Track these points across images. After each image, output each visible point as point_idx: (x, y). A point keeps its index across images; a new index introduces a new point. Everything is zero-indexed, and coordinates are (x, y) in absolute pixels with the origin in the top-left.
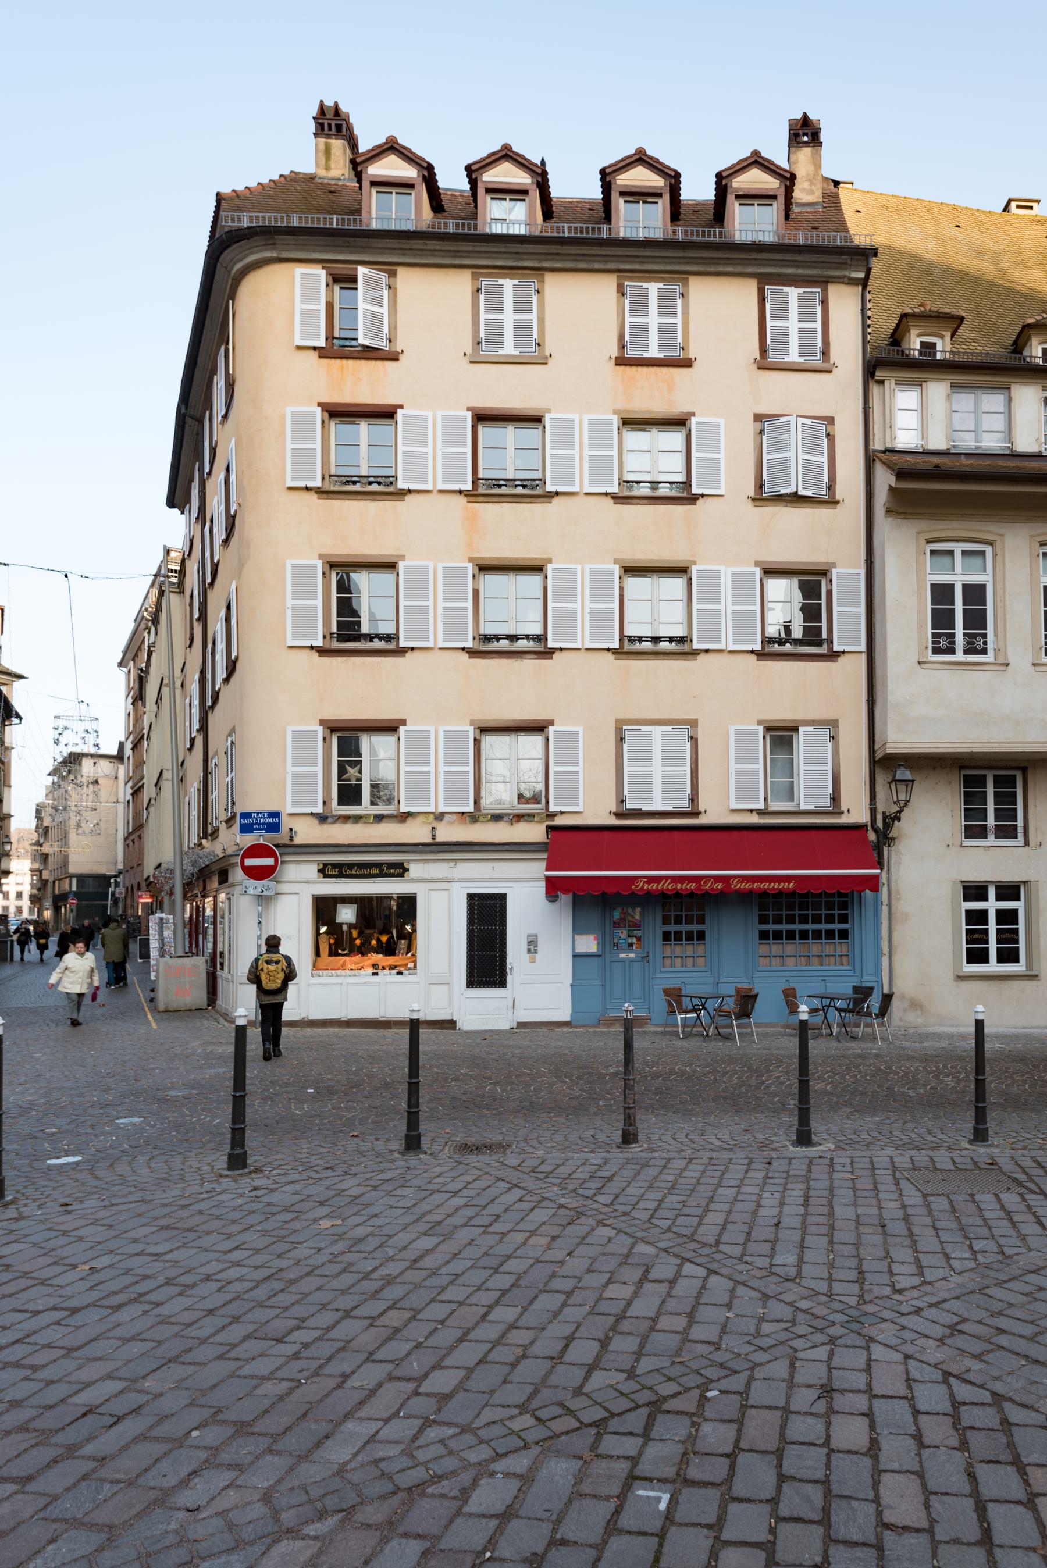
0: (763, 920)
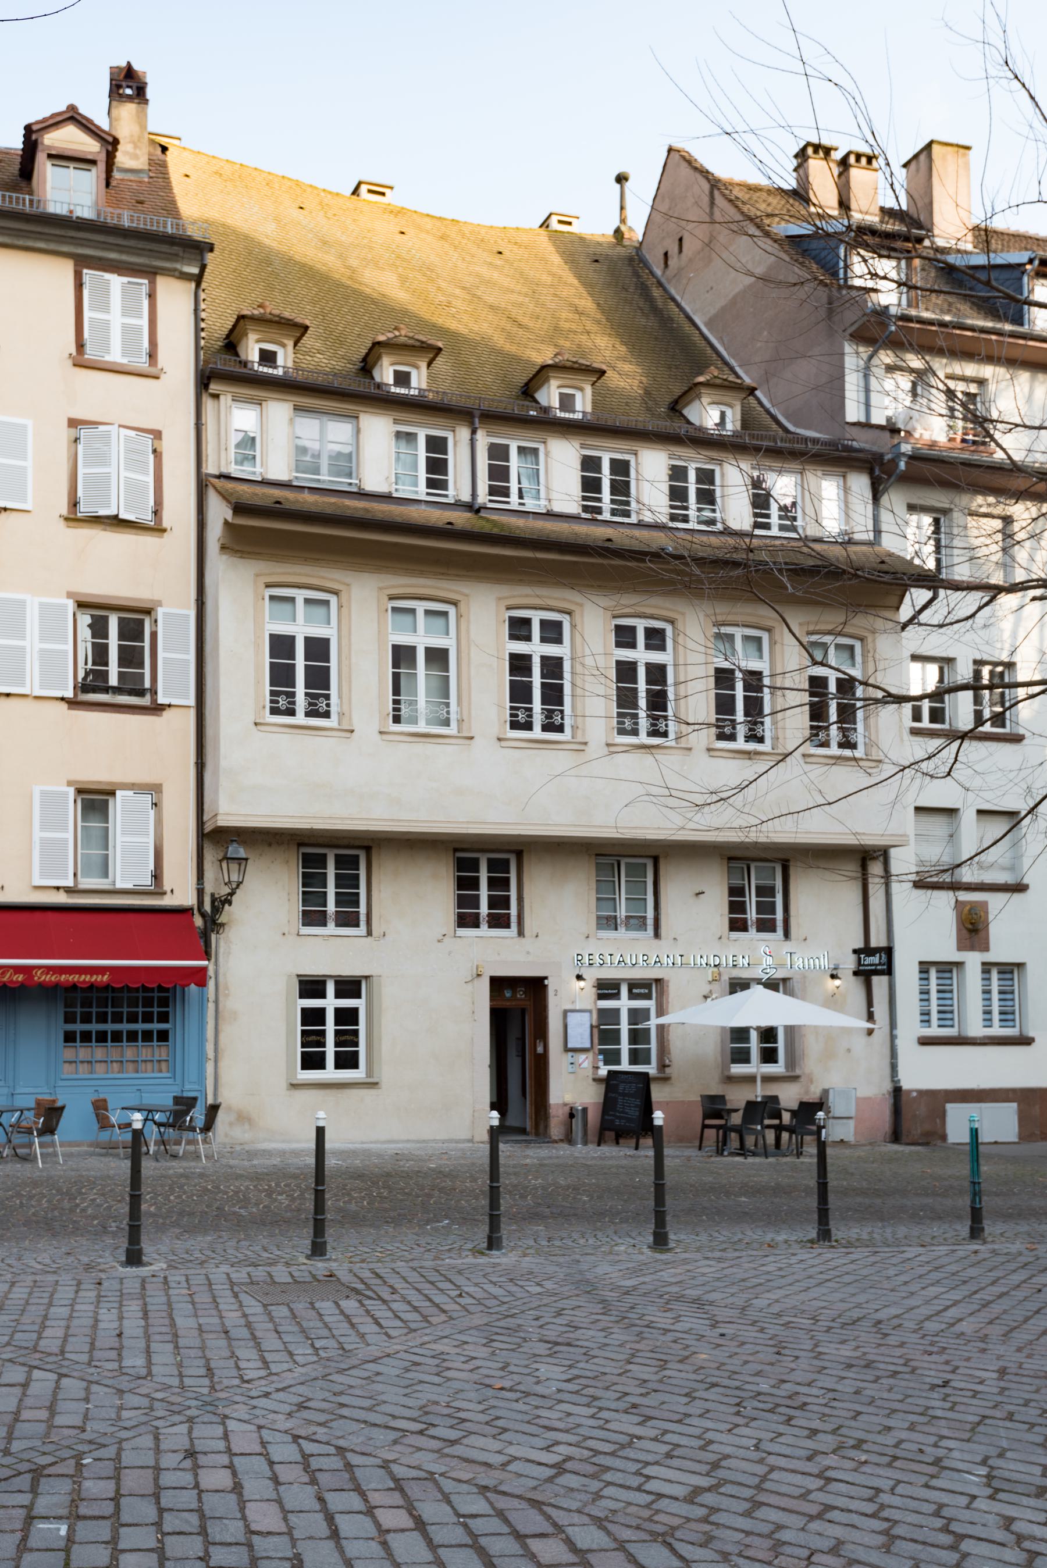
0: (69, 1019)
